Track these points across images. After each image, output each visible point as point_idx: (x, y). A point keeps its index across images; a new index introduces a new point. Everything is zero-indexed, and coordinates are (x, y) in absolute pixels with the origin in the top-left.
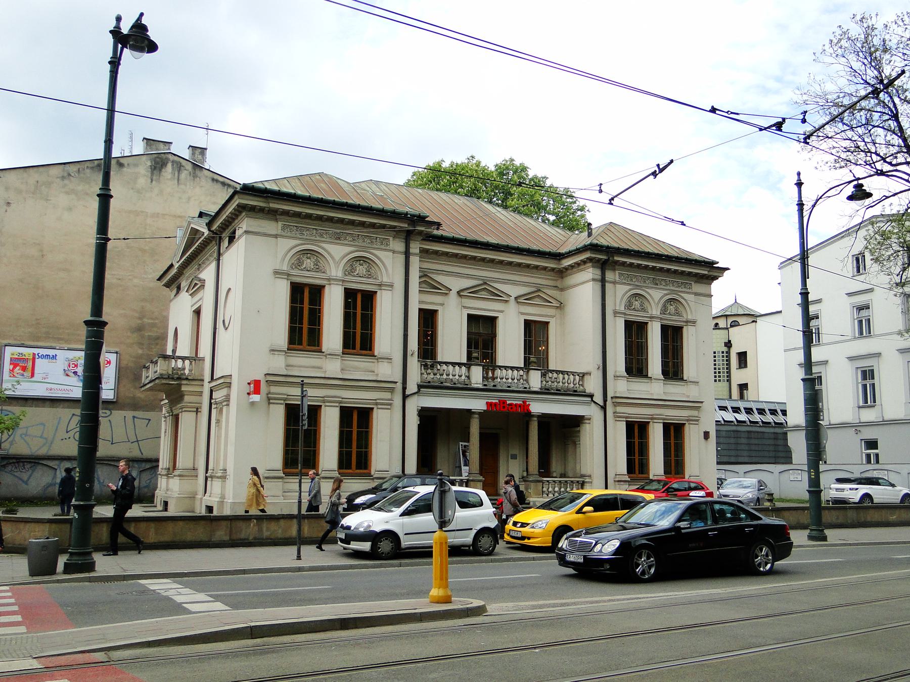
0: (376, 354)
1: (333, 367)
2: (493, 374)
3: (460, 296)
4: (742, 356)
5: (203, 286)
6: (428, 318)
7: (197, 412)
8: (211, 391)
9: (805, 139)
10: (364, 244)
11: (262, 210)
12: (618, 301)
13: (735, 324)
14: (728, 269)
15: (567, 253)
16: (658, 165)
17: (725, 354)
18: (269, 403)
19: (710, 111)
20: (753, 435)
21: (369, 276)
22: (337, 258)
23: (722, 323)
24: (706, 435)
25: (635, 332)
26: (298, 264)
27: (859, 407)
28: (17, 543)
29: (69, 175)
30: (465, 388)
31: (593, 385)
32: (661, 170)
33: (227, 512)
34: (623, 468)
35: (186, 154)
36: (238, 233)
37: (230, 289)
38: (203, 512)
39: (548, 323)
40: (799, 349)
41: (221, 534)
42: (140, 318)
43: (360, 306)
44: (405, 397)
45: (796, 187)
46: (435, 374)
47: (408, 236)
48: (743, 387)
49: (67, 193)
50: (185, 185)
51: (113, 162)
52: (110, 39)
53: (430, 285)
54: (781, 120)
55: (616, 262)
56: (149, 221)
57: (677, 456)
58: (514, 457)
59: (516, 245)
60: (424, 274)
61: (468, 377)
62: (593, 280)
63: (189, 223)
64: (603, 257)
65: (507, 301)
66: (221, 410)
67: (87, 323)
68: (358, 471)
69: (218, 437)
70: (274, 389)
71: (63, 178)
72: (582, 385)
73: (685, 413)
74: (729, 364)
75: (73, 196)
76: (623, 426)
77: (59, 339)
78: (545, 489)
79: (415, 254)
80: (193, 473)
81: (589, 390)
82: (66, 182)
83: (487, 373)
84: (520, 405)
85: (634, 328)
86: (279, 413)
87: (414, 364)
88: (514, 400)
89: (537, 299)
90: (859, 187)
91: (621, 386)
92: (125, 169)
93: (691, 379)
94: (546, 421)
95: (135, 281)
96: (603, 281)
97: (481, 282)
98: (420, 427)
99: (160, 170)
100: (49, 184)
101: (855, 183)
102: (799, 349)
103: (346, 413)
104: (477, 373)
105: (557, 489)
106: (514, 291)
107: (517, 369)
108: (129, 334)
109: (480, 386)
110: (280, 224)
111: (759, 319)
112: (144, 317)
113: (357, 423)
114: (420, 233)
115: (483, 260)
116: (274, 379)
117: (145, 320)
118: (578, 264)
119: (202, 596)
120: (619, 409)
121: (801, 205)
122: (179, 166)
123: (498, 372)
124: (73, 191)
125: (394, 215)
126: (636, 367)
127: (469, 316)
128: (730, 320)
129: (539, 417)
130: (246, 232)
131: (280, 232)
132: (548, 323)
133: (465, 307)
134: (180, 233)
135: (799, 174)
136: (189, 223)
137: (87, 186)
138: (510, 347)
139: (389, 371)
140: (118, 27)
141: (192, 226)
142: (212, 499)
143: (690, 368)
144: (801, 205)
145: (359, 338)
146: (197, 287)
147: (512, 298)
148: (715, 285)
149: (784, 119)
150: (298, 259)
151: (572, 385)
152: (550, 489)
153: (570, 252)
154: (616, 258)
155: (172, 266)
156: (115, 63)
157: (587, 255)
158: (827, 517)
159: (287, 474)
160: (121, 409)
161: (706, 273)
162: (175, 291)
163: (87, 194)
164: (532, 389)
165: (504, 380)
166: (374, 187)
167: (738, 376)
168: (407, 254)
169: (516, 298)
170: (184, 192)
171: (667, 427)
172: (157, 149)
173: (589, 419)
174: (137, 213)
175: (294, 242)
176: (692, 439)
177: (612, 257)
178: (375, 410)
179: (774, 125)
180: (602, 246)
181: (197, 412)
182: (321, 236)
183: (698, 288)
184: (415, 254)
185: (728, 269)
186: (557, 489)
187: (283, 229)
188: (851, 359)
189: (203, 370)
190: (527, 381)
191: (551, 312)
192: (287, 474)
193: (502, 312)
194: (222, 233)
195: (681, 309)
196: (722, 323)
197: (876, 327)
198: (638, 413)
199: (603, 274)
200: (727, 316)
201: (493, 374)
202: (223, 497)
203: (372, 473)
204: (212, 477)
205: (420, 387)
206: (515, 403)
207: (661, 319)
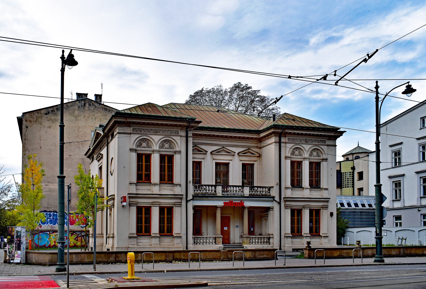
1: (156, 190)
2: (227, 189)
4: (361, 175)
5: (102, 157)
6: (197, 165)
7: (102, 210)
9: (336, 83)
10: (168, 134)
11: (124, 122)
12: (287, 152)
13: (357, 158)
15: (262, 130)
16: (368, 55)
17: (351, 173)
18: (130, 206)
19: (288, 78)
20: (363, 214)
21: (171, 148)
22: (156, 141)
23: (350, 157)
24: (332, 214)
25: (296, 166)
26: (139, 145)
27: (421, 198)
28: (39, 261)
30: (214, 196)
31: (274, 193)
32: (370, 57)
33: (115, 250)
34: (289, 231)
35: (93, 98)
36: (115, 133)
37: (112, 158)
38: (106, 251)
40: (382, 170)
41: (112, 259)
43: (167, 162)
44: (187, 201)
46: (200, 191)
47: (187, 129)
48: (360, 190)
49: (48, 120)
50: (94, 112)
51: (64, 105)
52: (60, 61)
53: (197, 150)
55: (287, 133)
57: (298, 224)
58: (237, 227)
59: (238, 128)
60: (195, 145)
61: (215, 191)
62: (275, 142)
63: (96, 130)
64: (280, 131)
65: (234, 155)
66: (111, 210)
67: (58, 177)
68: (167, 234)
69: (111, 221)
70: (132, 200)
71: (46, 114)
72: (269, 193)
73: (321, 204)
74: (353, 178)
75: (50, 122)
76: (289, 211)
78: (251, 241)
79: (190, 137)
80: (102, 236)
82: (48, 115)
83: (224, 189)
84: (239, 203)
86: (134, 210)
87: (191, 186)
88: (237, 201)
89: (248, 153)
94: (251, 210)
96: (280, 143)
97: (247, 149)
98: (193, 214)
101: (407, 84)
102: (382, 170)
104: (219, 189)
105: (257, 241)
106: (237, 150)
107: (239, 186)
109: (221, 195)
110: (132, 128)
111: (370, 155)
113: (167, 213)
114: (193, 127)
115: (222, 136)
116: (132, 196)
118: (268, 135)
119: (103, 280)
120: (287, 203)
121: (377, 98)
123: (229, 189)
125: (181, 119)
126: (296, 183)
128: (355, 156)
129: (248, 208)
130: (118, 133)
131: (132, 132)
133: (214, 159)
134: (93, 133)
136: (96, 130)
137: (56, 117)
138: (235, 177)
140: (63, 55)
141: (97, 131)
142: (109, 246)
144: (377, 98)
145: (167, 177)
146: (100, 158)
147: (236, 154)
149: (327, 75)
150: (140, 143)
152: (254, 241)
153: (264, 129)
154: (286, 131)
155: (90, 149)
156: (63, 70)
157: (272, 130)
158: (384, 252)
159: (138, 236)
161: (333, 134)
162: (91, 160)
164: (245, 196)
165: (232, 192)
166: (173, 107)
167: (358, 184)
168: (187, 137)
169: (238, 154)
171: (162, 210)
172: (82, 97)
173: (273, 208)
175: (137, 136)
176: (324, 216)
177: (289, 129)
178: (174, 207)
180: (279, 126)
182: (149, 132)
183: (329, 142)
186: (257, 241)
187: (133, 130)
188: (417, 173)
189: (104, 193)
190: (243, 192)
191: (255, 159)
192: (138, 236)
193: (231, 160)
194: (108, 134)
196: (350, 157)
197: (404, 160)
199: (280, 140)
200: (353, 154)
201: (227, 189)
202: (113, 245)
203: (174, 234)
204: (109, 237)
205: (193, 196)
206: (237, 202)
207: (309, 159)
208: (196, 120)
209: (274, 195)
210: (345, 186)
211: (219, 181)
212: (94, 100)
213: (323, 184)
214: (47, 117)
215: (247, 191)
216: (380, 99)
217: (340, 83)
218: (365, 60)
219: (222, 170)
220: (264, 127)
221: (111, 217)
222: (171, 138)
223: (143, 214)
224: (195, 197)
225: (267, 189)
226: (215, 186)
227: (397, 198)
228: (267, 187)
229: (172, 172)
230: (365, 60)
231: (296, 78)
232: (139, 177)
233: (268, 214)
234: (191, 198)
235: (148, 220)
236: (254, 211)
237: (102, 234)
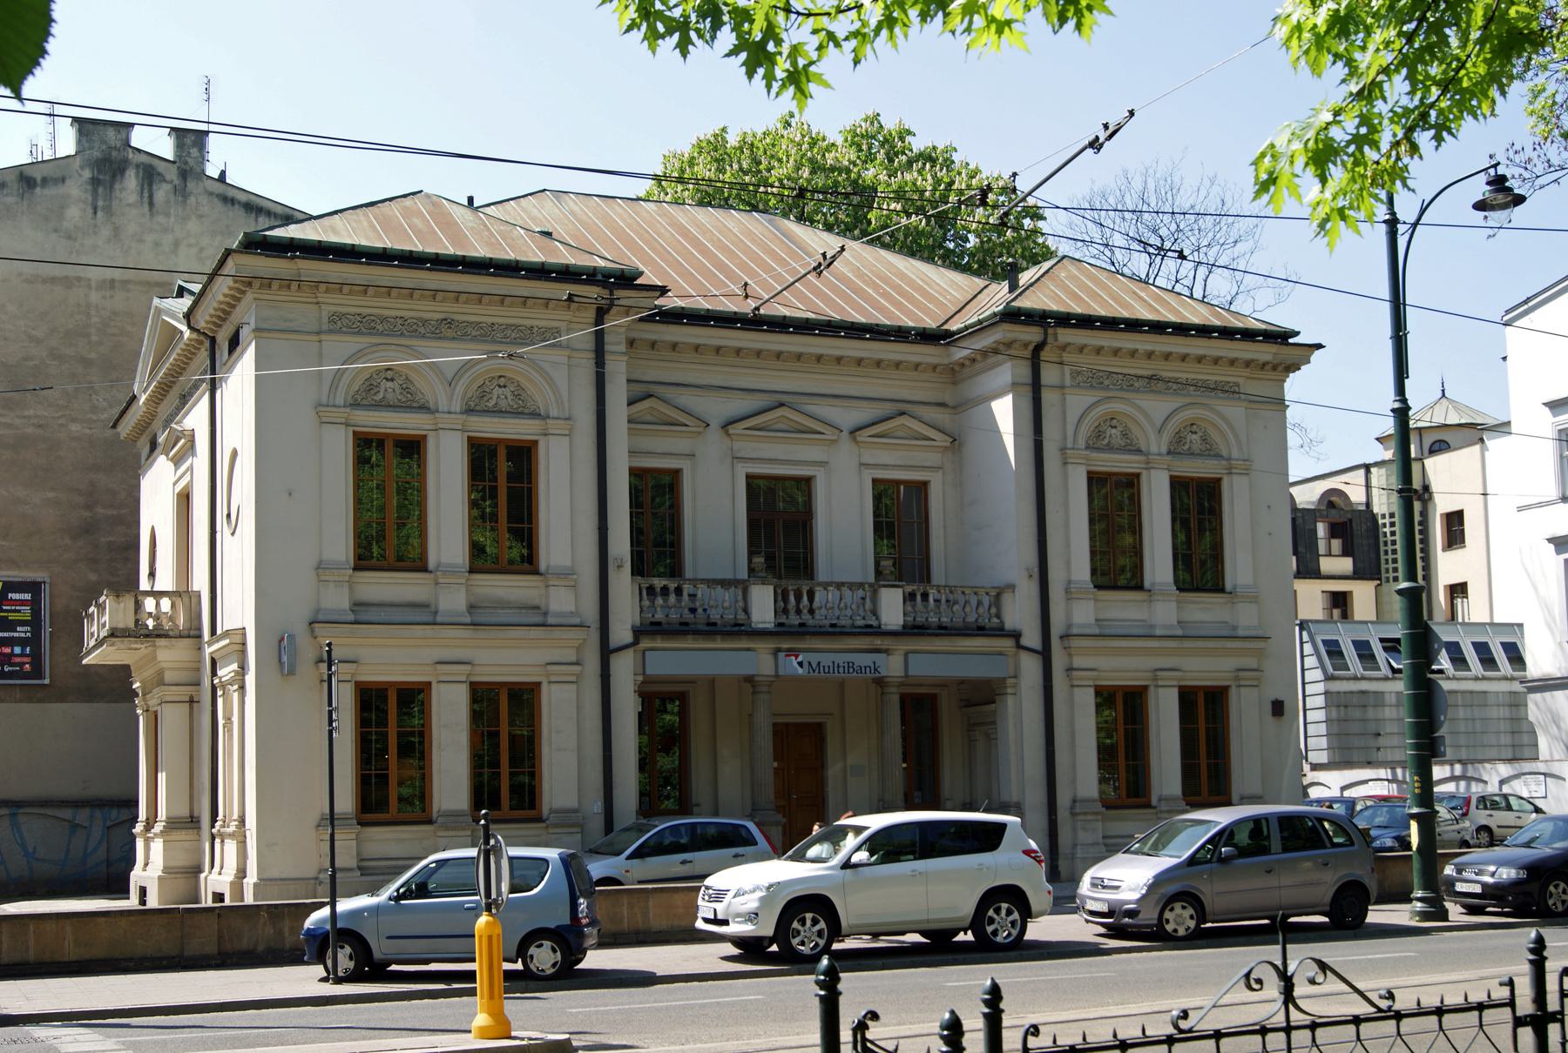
8: (214, 662)
14: (1319, 346)
15: (960, 331)
16: (1106, 126)
25: (1114, 501)
34: (1082, 570)
35: (163, 147)
42: (88, 507)
50: (167, 215)
54: (431, 405)
65: (834, 442)
72: (998, 616)
81: (1010, 623)
87: (623, 585)
90: (1499, 183)
91: (1081, 611)
92: (38, 190)
95: (74, 427)
99: (111, 187)
103: (1188, 698)
108: (68, 541)
109: (770, 626)
117: (100, 510)
121: (1392, 223)
122: (150, 169)
126: (1117, 567)
139: (570, 599)
143: (1238, 568)
147: (845, 434)
148: (1294, 386)
169: (852, 432)
170: (166, 230)
181: (191, 701)
185: (1319, 346)
191: (933, 458)
202: (242, 873)
205: (639, 633)
208: (638, 282)
209: (1018, 627)
212: (170, 157)
215: (892, 607)
216: (1401, 228)
218: (1095, 145)
220: (970, 317)
221: (231, 736)
229: (530, 522)
230: (1095, 145)
233: (994, 712)
234: (628, 637)
237: (1073, 814)
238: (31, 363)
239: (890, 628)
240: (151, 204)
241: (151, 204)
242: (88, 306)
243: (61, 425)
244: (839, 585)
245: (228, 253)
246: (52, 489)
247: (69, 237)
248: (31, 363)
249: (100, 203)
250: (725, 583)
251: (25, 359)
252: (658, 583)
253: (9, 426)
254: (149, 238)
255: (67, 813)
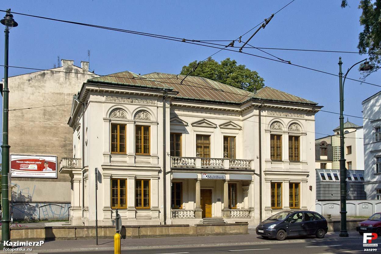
0: (151, 155)
3: (193, 126)
9: (240, 50)
24: (311, 188)
25: (276, 138)
29: (32, 79)
31: (254, 166)
34: (269, 204)
39: (235, 137)
42: (65, 141)
43: (143, 132)
44: (165, 174)
45: (338, 65)
47: (163, 99)
49: (31, 87)
50: (81, 80)
56: (66, 97)
75: (34, 88)
77: (32, 152)
79: (168, 107)
81: (253, 169)
83: (204, 162)
85: (175, 135)
87: (168, 158)
92: (54, 74)
93: (303, 161)
95: (62, 125)
97: (203, 119)
100: (23, 83)
106: (218, 122)
108: (61, 148)
112: (66, 140)
113: (143, 186)
124: (34, 86)
126: (276, 156)
127: (197, 135)
132: (235, 137)
135: (340, 59)
138: (217, 149)
145: (143, 148)
149: (234, 41)
151: (245, 166)
155: (71, 118)
160: (60, 181)
163: (40, 87)
169: (220, 126)
174: (60, 94)
176: (303, 188)
179: (230, 45)
184: (168, 107)
191: (237, 131)
195: (299, 127)
198: (276, 178)
201: (209, 162)
205: (172, 169)
207: (289, 133)
209: (10, 146)
210: (335, 160)
211: (226, 155)
213: (302, 158)
214: (30, 84)
217: (244, 50)
219: (203, 142)
222: (281, 120)
223: (118, 186)
224: (174, 169)
225: (247, 163)
226: (223, 160)
227: (378, 172)
228: (248, 161)
231: (192, 42)
232: (113, 149)
235: (123, 193)
236: (236, 184)
238: (53, 111)
239: (226, 169)
240: (77, 77)
241: (77, 77)
242: (65, 99)
243: (59, 124)
244: (215, 159)
245: (84, 84)
246: (58, 137)
247: (61, 84)
248: (53, 111)
249: (67, 77)
250: (191, 158)
251: (52, 110)
252: (176, 158)
253: (49, 124)
254: (77, 85)
255: (60, 205)
